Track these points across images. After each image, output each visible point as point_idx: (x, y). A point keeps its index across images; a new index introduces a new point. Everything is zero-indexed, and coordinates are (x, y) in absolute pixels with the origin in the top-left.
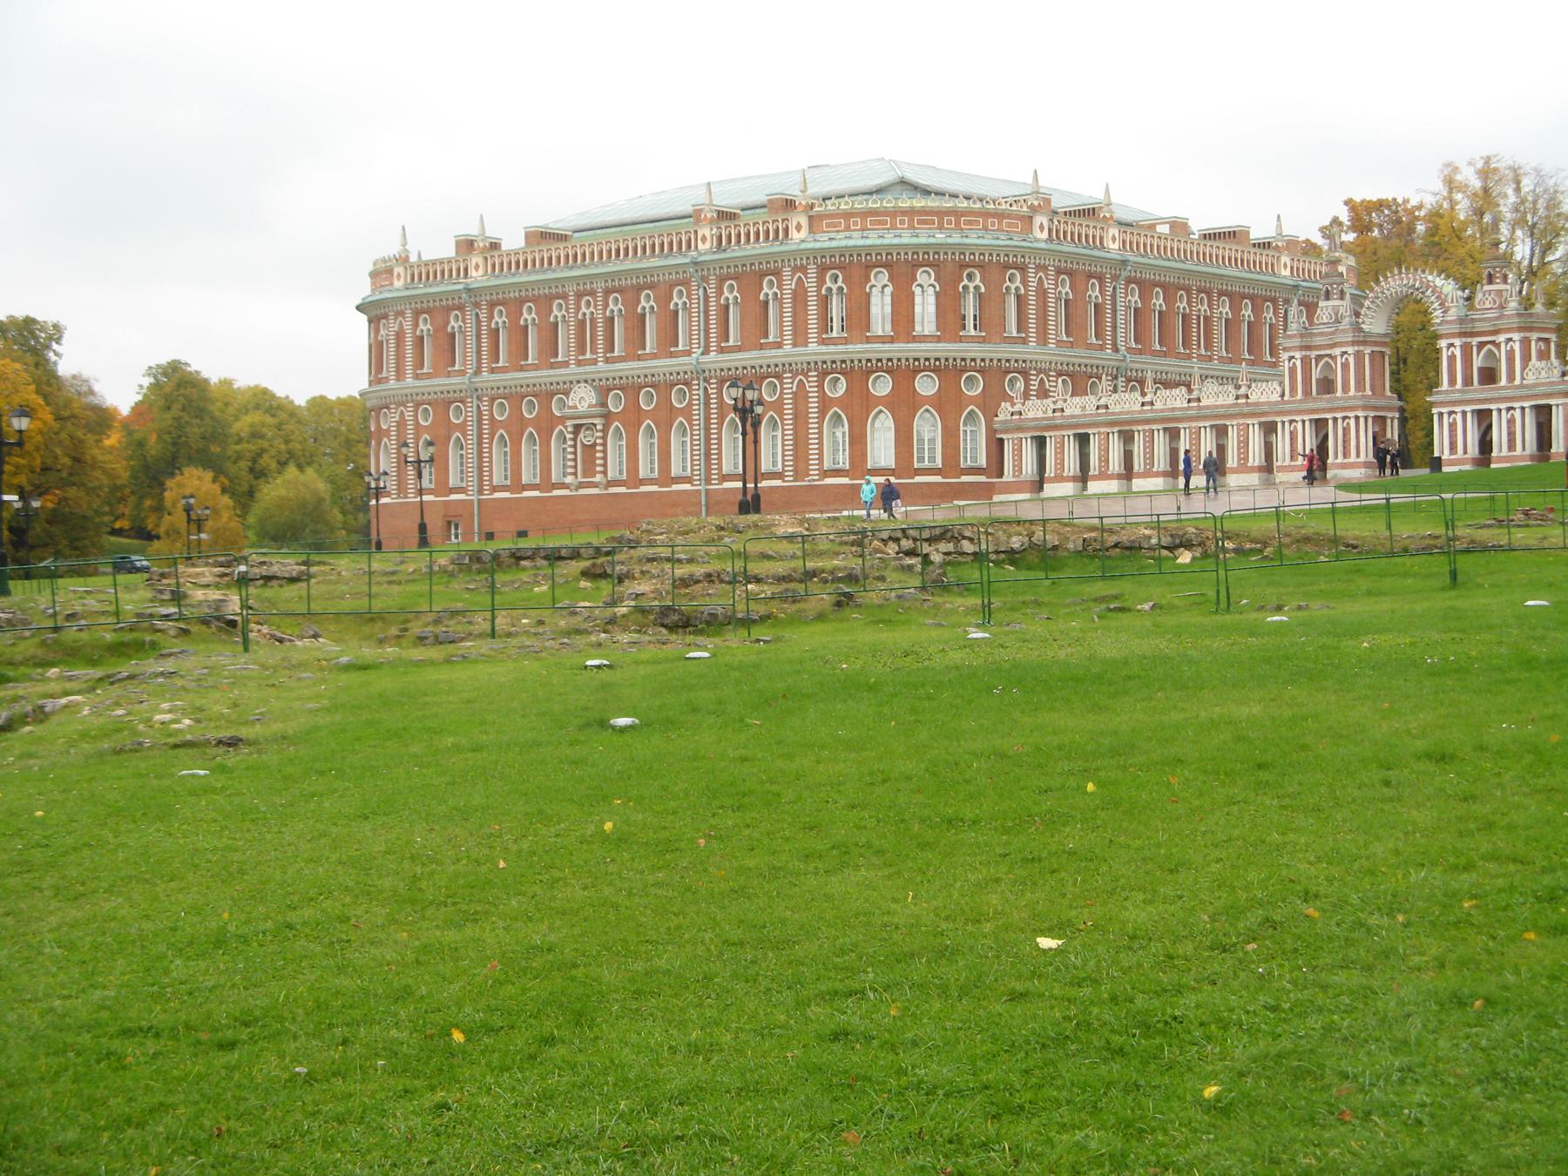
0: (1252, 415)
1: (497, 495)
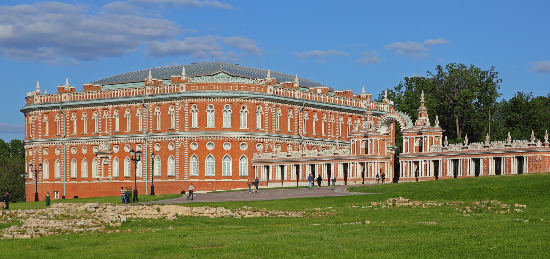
0: (467, 155)
1: (72, 182)
